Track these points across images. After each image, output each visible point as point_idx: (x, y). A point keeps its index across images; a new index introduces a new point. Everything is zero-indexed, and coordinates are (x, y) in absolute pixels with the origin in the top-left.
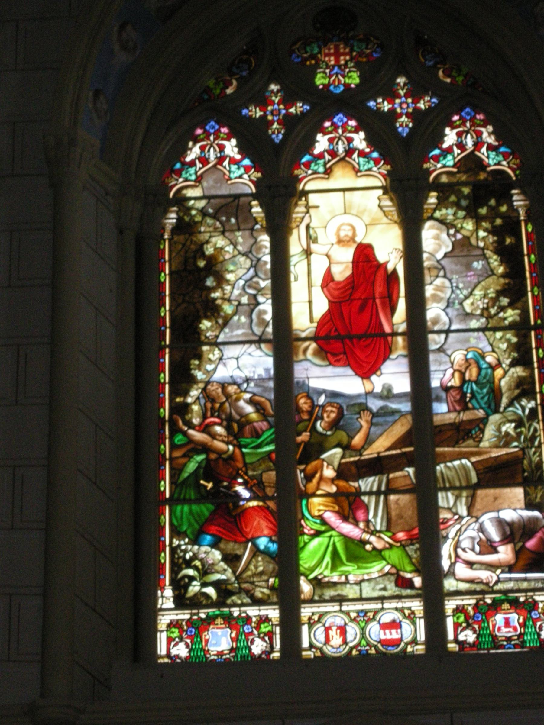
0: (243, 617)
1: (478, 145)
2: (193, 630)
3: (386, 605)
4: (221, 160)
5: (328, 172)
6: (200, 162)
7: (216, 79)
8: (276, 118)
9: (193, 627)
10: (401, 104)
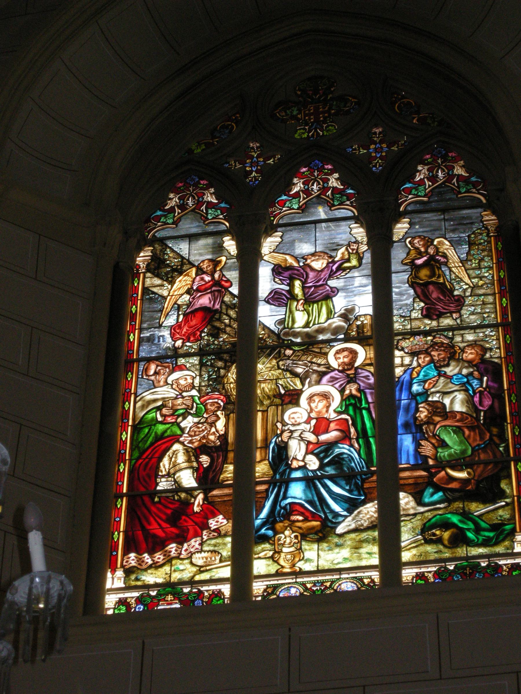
0: (195, 593)
1: (450, 177)
2: (142, 607)
3: (343, 576)
4: (199, 204)
5: (176, 223)
6: (429, 180)
7: (198, 142)
8: (254, 169)
9: (143, 604)
10: (375, 149)
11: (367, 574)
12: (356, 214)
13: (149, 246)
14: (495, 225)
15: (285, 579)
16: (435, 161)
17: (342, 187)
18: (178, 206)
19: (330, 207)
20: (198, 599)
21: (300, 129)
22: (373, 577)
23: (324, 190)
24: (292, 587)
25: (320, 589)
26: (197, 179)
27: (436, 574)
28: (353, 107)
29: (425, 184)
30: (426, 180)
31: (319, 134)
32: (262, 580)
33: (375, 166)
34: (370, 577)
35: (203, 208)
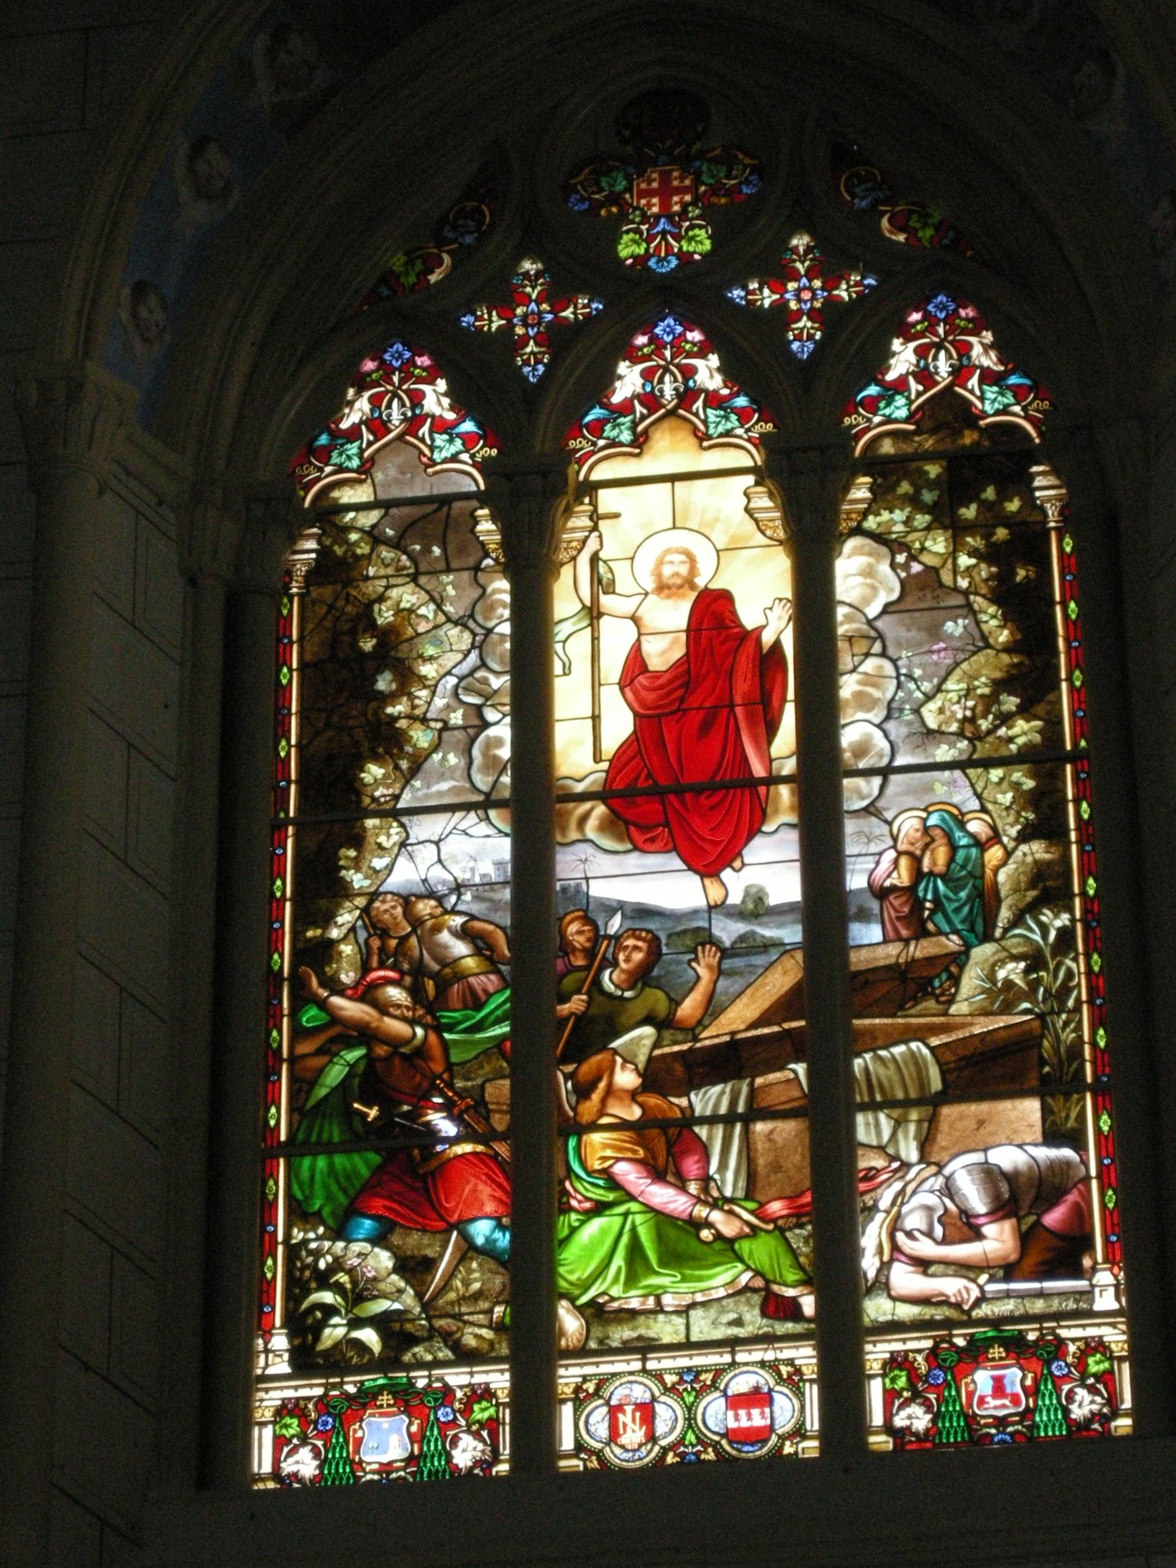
1: (960, 373)
3: (741, 1357)
7: (407, 254)
11: (787, 1354)
12: (482, 487)
13: (865, 475)
14: (1060, 500)
15: (612, 1362)
16: (931, 330)
17: (1002, 368)
18: (914, 374)
19: (701, 440)
20: (443, 1405)
21: (627, 232)
22: (797, 1362)
23: (686, 397)
24: (636, 1382)
25: (693, 1388)
26: (407, 355)
27: (933, 1355)
28: (747, 179)
29: (909, 390)
30: (363, 428)
31: (672, 247)
32: (595, 1360)
33: (798, 338)
34: (790, 1362)
35: (973, 382)
